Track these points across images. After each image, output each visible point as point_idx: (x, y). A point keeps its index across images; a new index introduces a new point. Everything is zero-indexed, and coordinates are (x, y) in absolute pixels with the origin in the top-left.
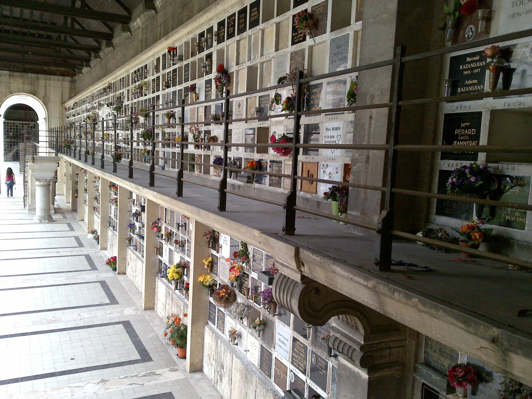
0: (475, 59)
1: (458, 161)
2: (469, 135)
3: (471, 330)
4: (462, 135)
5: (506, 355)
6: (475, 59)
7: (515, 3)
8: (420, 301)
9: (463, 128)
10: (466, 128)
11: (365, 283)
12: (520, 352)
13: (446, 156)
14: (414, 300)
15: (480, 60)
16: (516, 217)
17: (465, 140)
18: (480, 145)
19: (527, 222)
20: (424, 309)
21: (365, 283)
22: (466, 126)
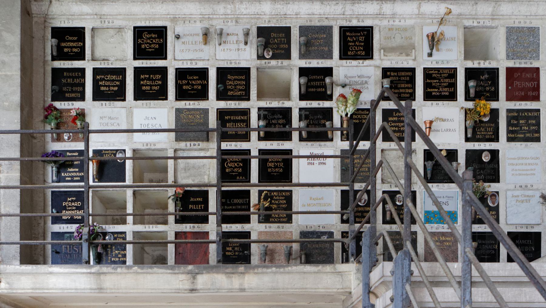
0: (74, 154)
1: (68, 225)
2: (76, 206)
3: (176, 271)
4: (70, 206)
5: (194, 278)
6: (74, 154)
7: (102, 124)
8: (139, 267)
9: (69, 201)
10: (72, 201)
11: (89, 271)
12: (204, 272)
13: (56, 220)
14: (134, 268)
15: (79, 156)
16: (119, 258)
17: (73, 210)
18: (340, 132)
19: (127, 260)
20: (142, 271)
21: (89, 271)
22: (72, 200)
